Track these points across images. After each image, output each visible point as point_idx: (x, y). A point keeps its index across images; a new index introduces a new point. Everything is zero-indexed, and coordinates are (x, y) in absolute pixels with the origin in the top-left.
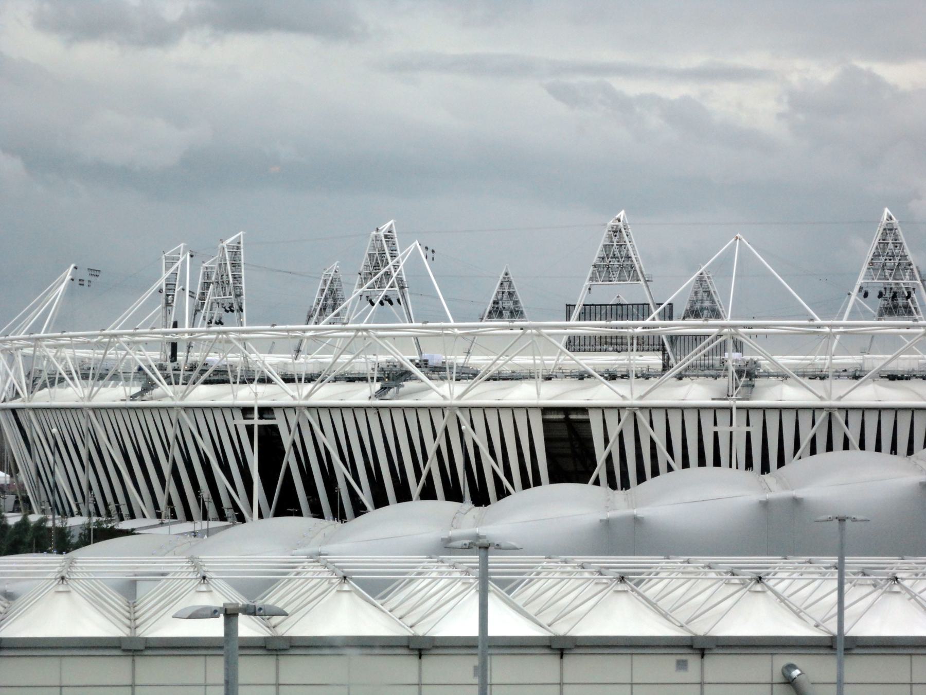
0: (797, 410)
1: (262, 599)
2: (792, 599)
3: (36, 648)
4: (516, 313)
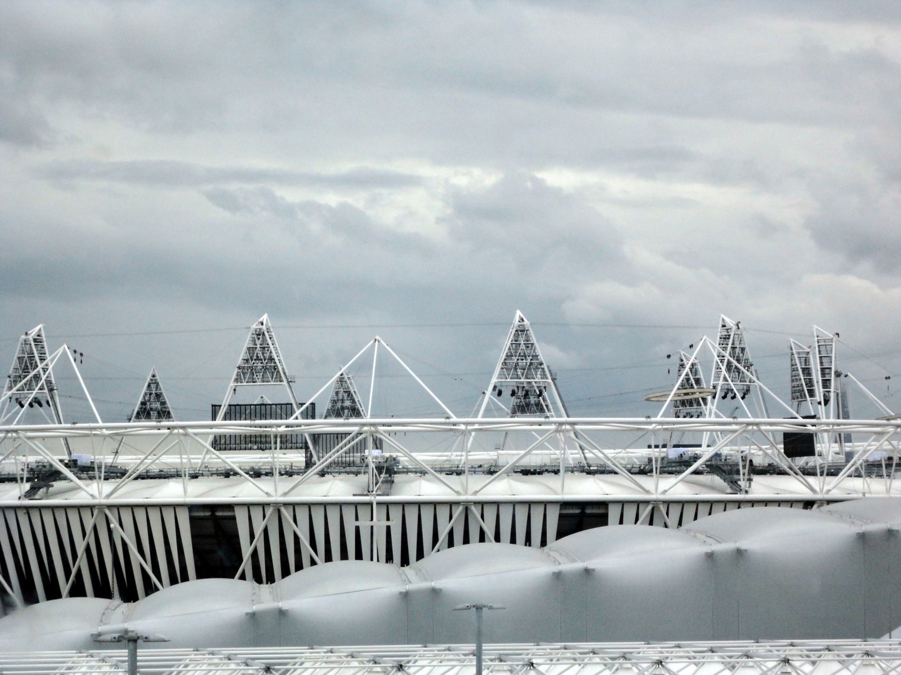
0: (435, 504)
4: (164, 414)
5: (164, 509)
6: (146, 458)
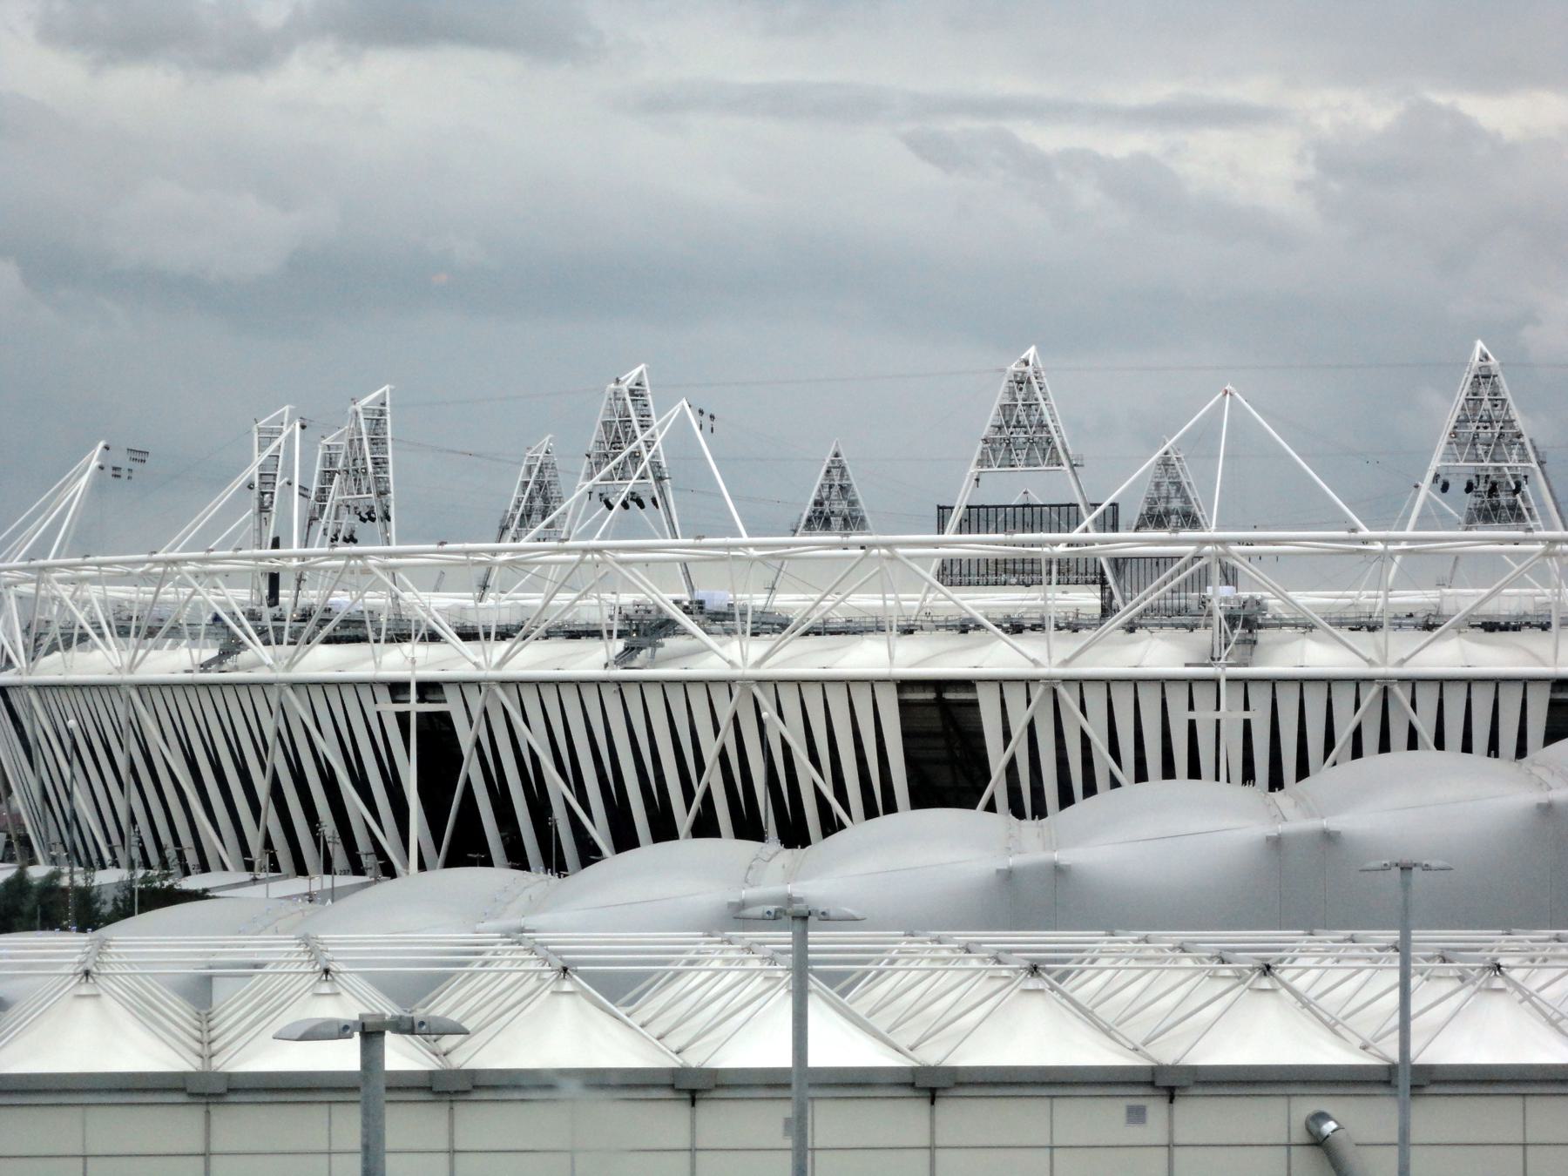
0: (1329, 682)
1: (424, 1006)
2: (1321, 1002)
4: (852, 522)
6: (822, 599)
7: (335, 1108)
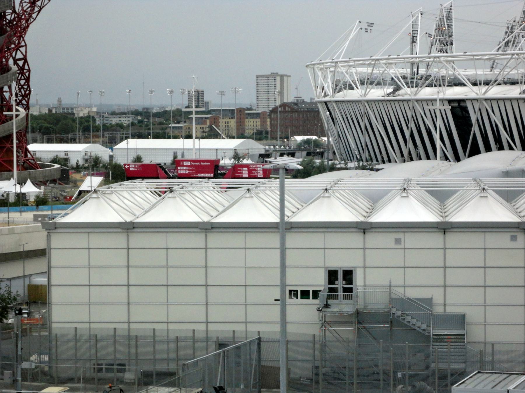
1: (515, 202)
3: (239, 228)
5: (492, 101)
6: (511, 71)
7: (247, 234)
